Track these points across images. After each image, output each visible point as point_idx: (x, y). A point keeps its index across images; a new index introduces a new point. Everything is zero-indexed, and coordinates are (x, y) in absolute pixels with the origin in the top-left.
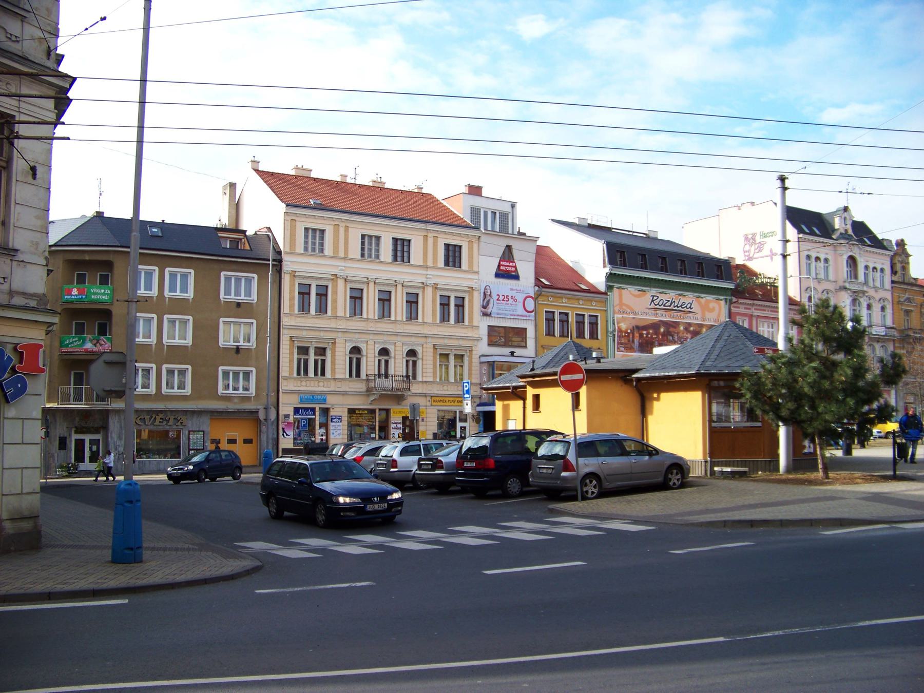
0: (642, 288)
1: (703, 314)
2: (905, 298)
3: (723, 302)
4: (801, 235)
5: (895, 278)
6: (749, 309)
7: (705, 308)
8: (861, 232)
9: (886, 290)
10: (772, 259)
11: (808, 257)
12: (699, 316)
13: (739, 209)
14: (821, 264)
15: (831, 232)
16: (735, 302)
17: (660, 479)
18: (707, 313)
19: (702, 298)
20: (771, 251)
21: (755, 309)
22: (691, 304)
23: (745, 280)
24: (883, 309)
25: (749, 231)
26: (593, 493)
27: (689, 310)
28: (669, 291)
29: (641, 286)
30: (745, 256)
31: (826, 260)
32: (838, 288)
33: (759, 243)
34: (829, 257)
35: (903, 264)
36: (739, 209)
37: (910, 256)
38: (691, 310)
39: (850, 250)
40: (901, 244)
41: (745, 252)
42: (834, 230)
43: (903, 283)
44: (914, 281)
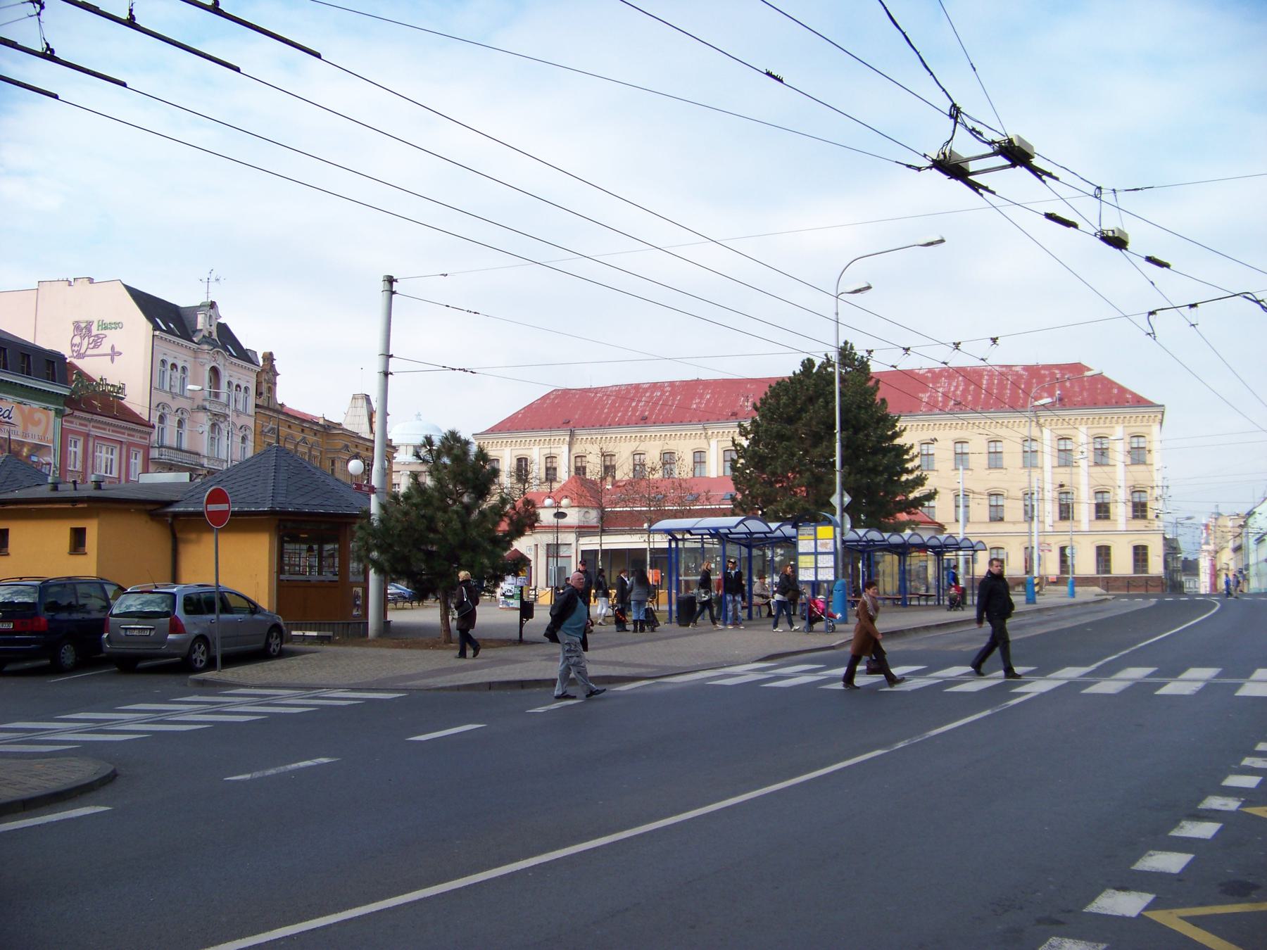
0: (48, 405)
1: (25, 428)
2: (268, 428)
3: (52, 414)
4: (157, 333)
5: (260, 402)
6: (86, 426)
7: (29, 419)
8: (225, 338)
9: (249, 416)
10: (112, 360)
11: (163, 362)
12: (20, 429)
13: (70, 285)
14: (178, 374)
15: (191, 334)
16: (68, 415)
17: (261, 645)
18: (30, 426)
19: (25, 404)
20: (113, 348)
21: (93, 427)
22: (10, 412)
23: (82, 386)
24: (244, 439)
25: (83, 317)
26: (201, 661)
27: (7, 420)
28: (31, 401)
29: (46, 402)
30: (73, 351)
31: (184, 369)
32: (196, 407)
33: (95, 336)
34: (188, 366)
35: (270, 385)
36: (70, 285)
37: (278, 374)
38: (9, 421)
39: (213, 359)
40: (269, 358)
41: (72, 345)
42: (195, 331)
43: (268, 408)
44: (279, 407)
